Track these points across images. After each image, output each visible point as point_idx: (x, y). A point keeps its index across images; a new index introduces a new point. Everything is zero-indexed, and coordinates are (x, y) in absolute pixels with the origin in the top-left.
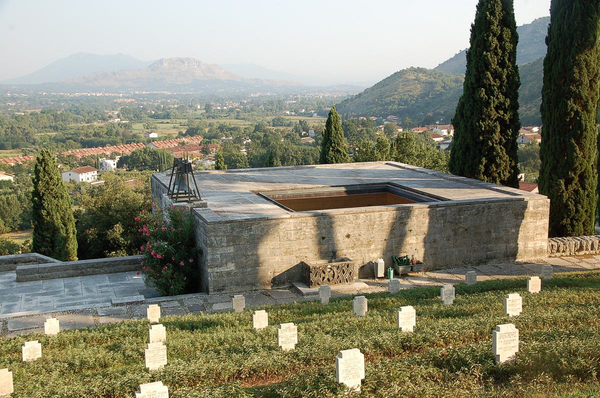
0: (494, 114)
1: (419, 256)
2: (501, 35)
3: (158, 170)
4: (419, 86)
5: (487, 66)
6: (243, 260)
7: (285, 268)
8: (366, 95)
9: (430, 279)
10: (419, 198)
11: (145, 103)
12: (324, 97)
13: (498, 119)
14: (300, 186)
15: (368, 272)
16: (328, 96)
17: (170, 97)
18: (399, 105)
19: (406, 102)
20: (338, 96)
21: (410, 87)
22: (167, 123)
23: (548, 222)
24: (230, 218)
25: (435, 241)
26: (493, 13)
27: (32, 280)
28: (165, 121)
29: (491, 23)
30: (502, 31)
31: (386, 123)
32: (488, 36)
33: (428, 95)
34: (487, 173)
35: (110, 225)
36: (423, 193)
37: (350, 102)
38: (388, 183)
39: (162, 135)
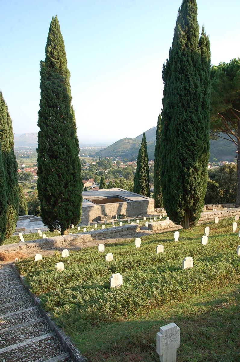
0: (143, 178)
1: (125, 214)
2: (144, 159)
4: (129, 145)
5: (141, 166)
6: (86, 215)
7: (95, 217)
9: (140, 217)
10: (125, 200)
11: (18, 152)
12: (91, 149)
13: (144, 179)
14: (96, 197)
15: (114, 218)
16: (93, 149)
18: (122, 152)
19: (124, 152)
20: (97, 148)
21: (126, 146)
23: (154, 206)
24: (83, 207)
25: (129, 210)
26: (142, 154)
28: (27, 159)
29: (142, 156)
30: (145, 158)
31: (117, 160)
33: (133, 149)
37: (102, 151)
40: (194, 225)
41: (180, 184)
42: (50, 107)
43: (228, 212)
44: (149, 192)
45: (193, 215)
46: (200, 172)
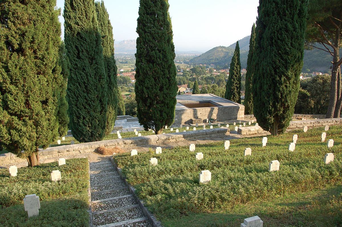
0: (235, 85)
1: (216, 118)
2: (237, 67)
3: (125, 84)
4: (223, 53)
5: (234, 74)
8: (203, 56)
10: (216, 105)
11: (118, 57)
12: (186, 56)
14: (189, 101)
15: (205, 121)
17: (127, 55)
19: (218, 59)
22: (127, 65)
27: (130, 121)
28: (126, 64)
31: (210, 67)
32: (234, 67)
33: (226, 57)
34: (233, 99)
35: (134, 108)
36: (217, 104)
38: (210, 101)
39: (125, 70)
40: (282, 133)
41: (271, 91)
42: (148, 14)
43: (317, 122)
44: (240, 99)
45: (282, 122)
46: (292, 81)
